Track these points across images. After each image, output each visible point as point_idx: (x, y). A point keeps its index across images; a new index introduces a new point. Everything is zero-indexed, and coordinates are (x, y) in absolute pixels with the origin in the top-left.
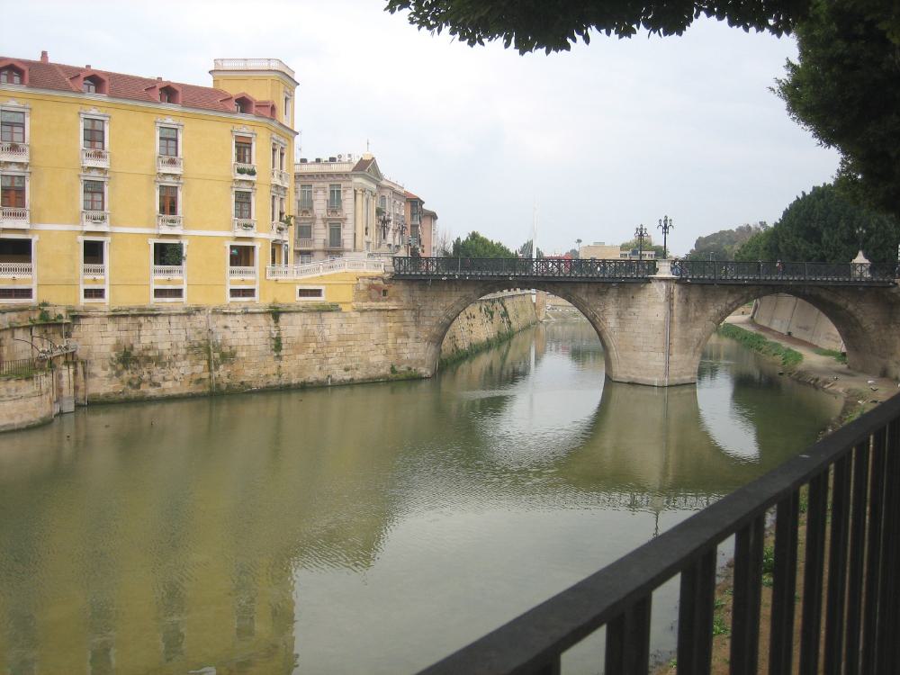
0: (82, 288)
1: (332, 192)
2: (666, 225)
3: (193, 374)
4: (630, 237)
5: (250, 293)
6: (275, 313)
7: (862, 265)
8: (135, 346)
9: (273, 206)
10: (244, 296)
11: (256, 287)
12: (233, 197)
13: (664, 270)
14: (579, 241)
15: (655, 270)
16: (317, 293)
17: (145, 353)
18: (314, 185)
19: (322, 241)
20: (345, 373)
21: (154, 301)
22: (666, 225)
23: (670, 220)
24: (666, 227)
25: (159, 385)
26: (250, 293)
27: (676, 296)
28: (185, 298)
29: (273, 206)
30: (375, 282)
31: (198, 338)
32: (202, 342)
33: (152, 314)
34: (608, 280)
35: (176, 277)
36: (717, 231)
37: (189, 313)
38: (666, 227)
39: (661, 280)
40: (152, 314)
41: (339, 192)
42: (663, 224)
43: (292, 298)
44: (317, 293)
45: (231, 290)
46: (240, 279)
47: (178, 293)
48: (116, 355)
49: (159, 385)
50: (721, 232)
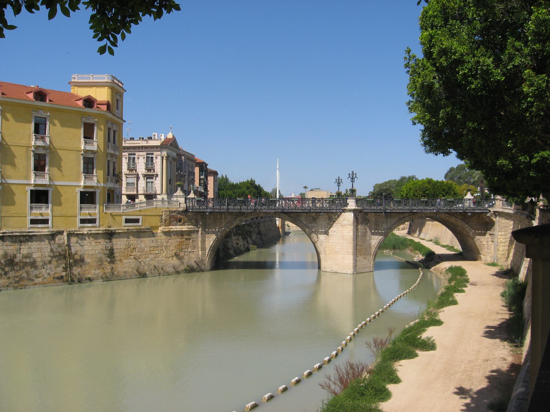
0: (29, 218)
1: (129, 159)
2: (353, 177)
3: (55, 273)
4: (442, 180)
5: (93, 221)
6: (110, 235)
7: (469, 199)
8: (18, 255)
9: (108, 167)
10: (89, 223)
11: (97, 217)
12: (82, 162)
13: (352, 204)
14: (306, 187)
15: (347, 205)
16: (137, 221)
17: (24, 260)
18: (137, 153)
19: (142, 189)
20: (161, 269)
21: (28, 228)
22: (353, 177)
23: (356, 174)
24: (353, 178)
25: (33, 280)
26: (93, 221)
27: (359, 217)
28: (140, 223)
29: (108, 167)
30: (173, 214)
31: (60, 250)
32: (62, 253)
33: (29, 238)
34: (318, 211)
35: (44, 211)
36: (387, 181)
37: (53, 236)
38: (353, 178)
39: (350, 211)
40: (29, 238)
41: (134, 158)
42: (351, 176)
43: (121, 226)
44: (137, 221)
45: (81, 219)
46: (88, 211)
47: (46, 221)
48: (5, 261)
49: (33, 280)
50: (403, 179)
